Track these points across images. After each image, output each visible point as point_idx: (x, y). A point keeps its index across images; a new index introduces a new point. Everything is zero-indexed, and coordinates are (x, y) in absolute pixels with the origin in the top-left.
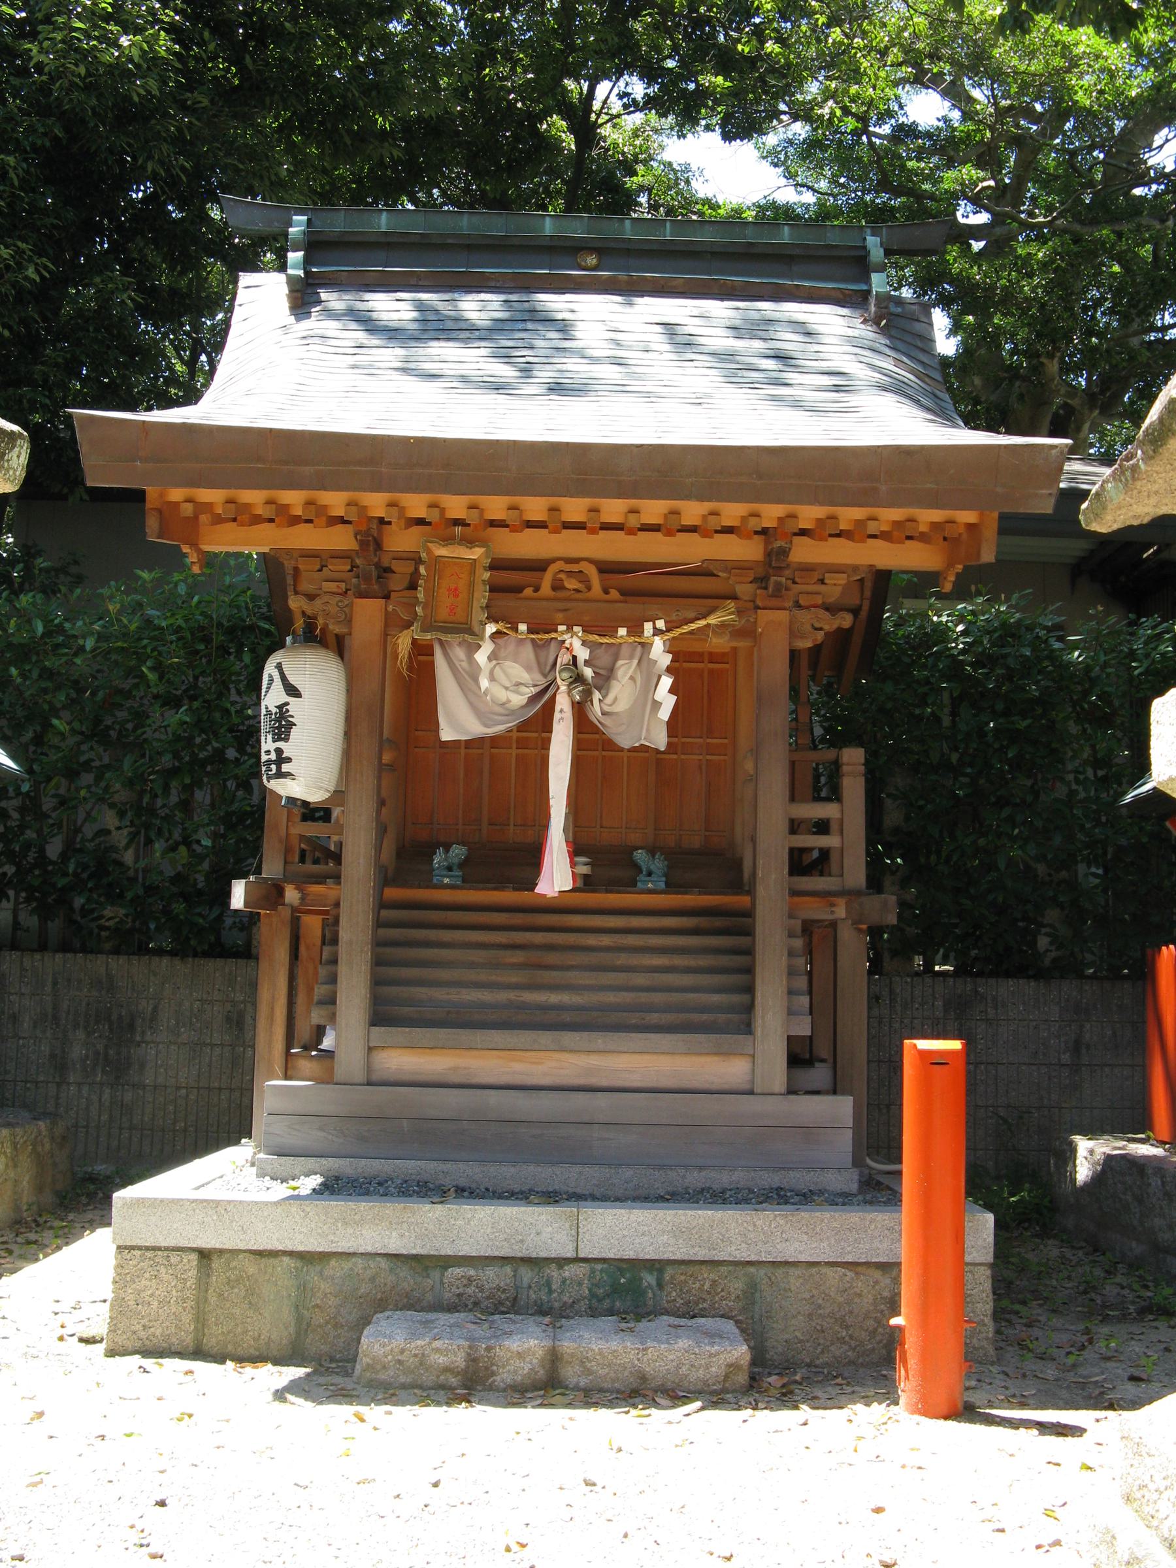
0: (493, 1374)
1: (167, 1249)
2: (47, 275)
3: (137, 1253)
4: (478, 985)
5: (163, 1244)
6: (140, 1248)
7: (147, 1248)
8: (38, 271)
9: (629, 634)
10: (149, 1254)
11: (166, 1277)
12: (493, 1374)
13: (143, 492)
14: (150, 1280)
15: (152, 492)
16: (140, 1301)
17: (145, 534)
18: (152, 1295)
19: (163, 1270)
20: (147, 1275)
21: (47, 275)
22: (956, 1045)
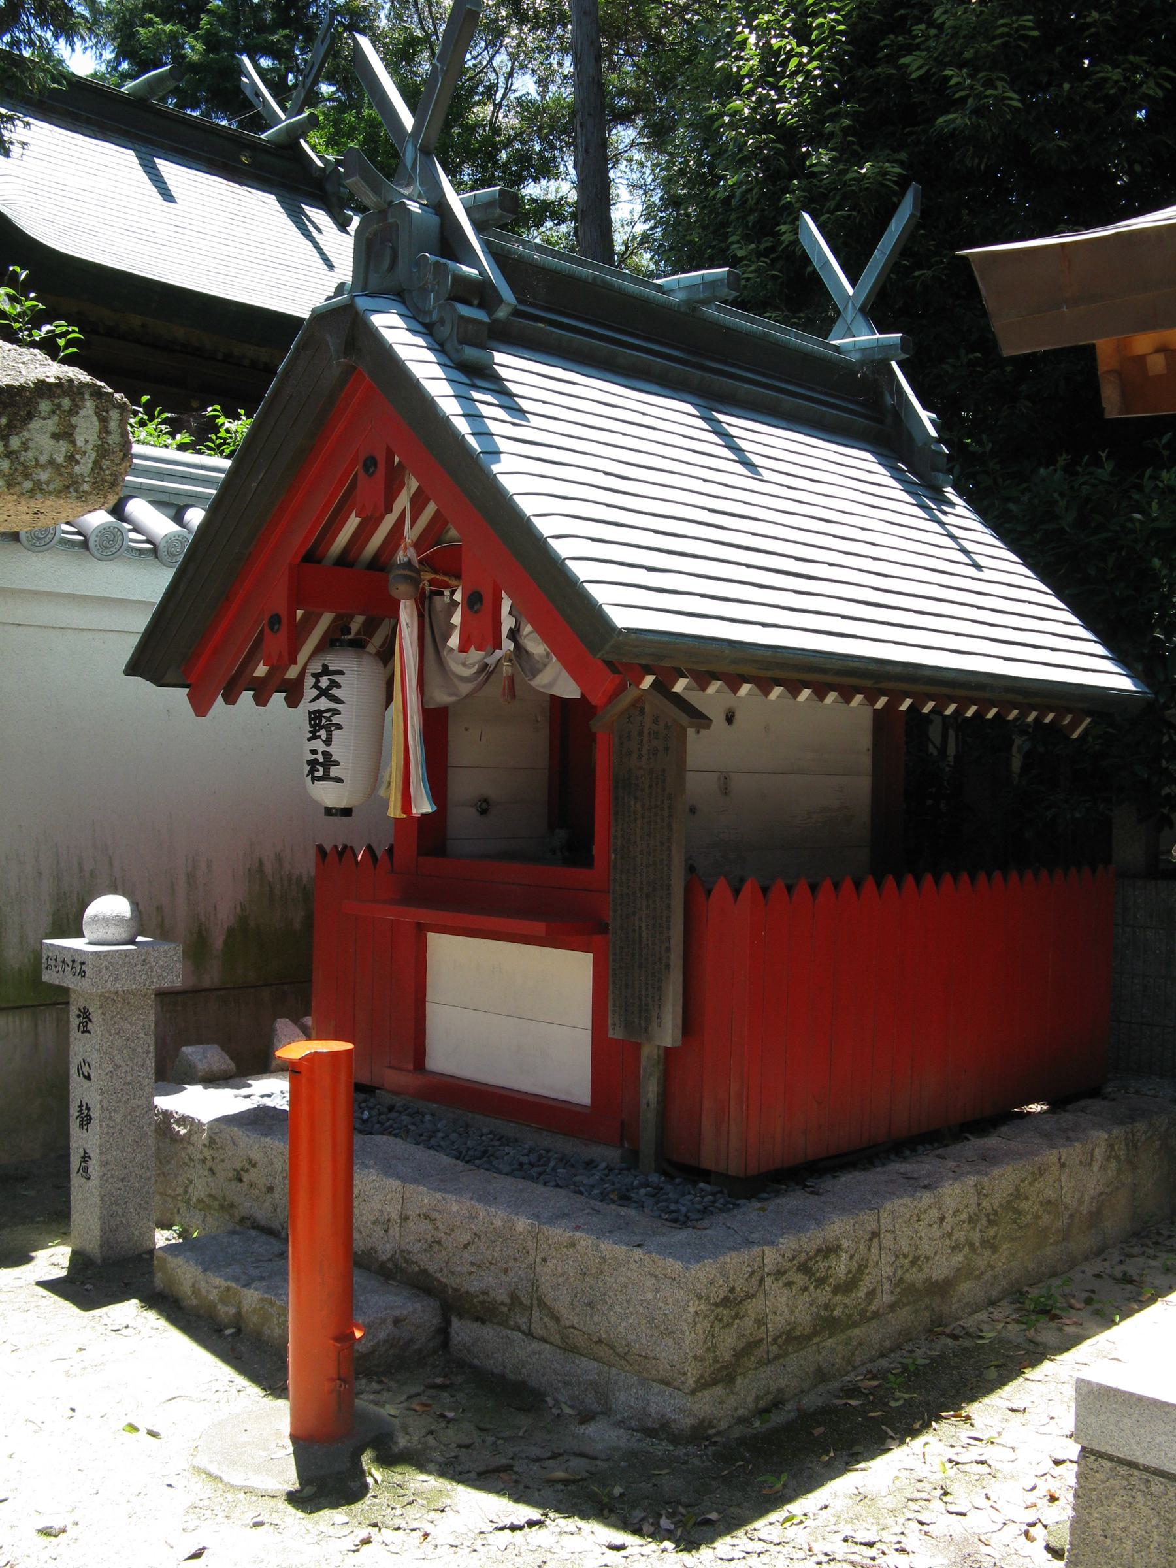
0: (300, 878)
1: (1146, 1469)
2: (1169, 86)
3: (1107, 1464)
4: (202, 467)
5: (1141, 1461)
6: (1110, 1458)
7: (1121, 1461)
8: (1159, 85)
9: (176, 105)
10: (1123, 1470)
11: (1146, 1511)
12: (300, 878)
13: (1091, 348)
14: (1123, 1508)
15: (1105, 347)
16: (1109, 1533)
17: (1102, 410)
18: (1124, 1529)
19: (1140, 1498)
20: (1119, 1499)
21: (1169, 86)
22: (1075, 736)
